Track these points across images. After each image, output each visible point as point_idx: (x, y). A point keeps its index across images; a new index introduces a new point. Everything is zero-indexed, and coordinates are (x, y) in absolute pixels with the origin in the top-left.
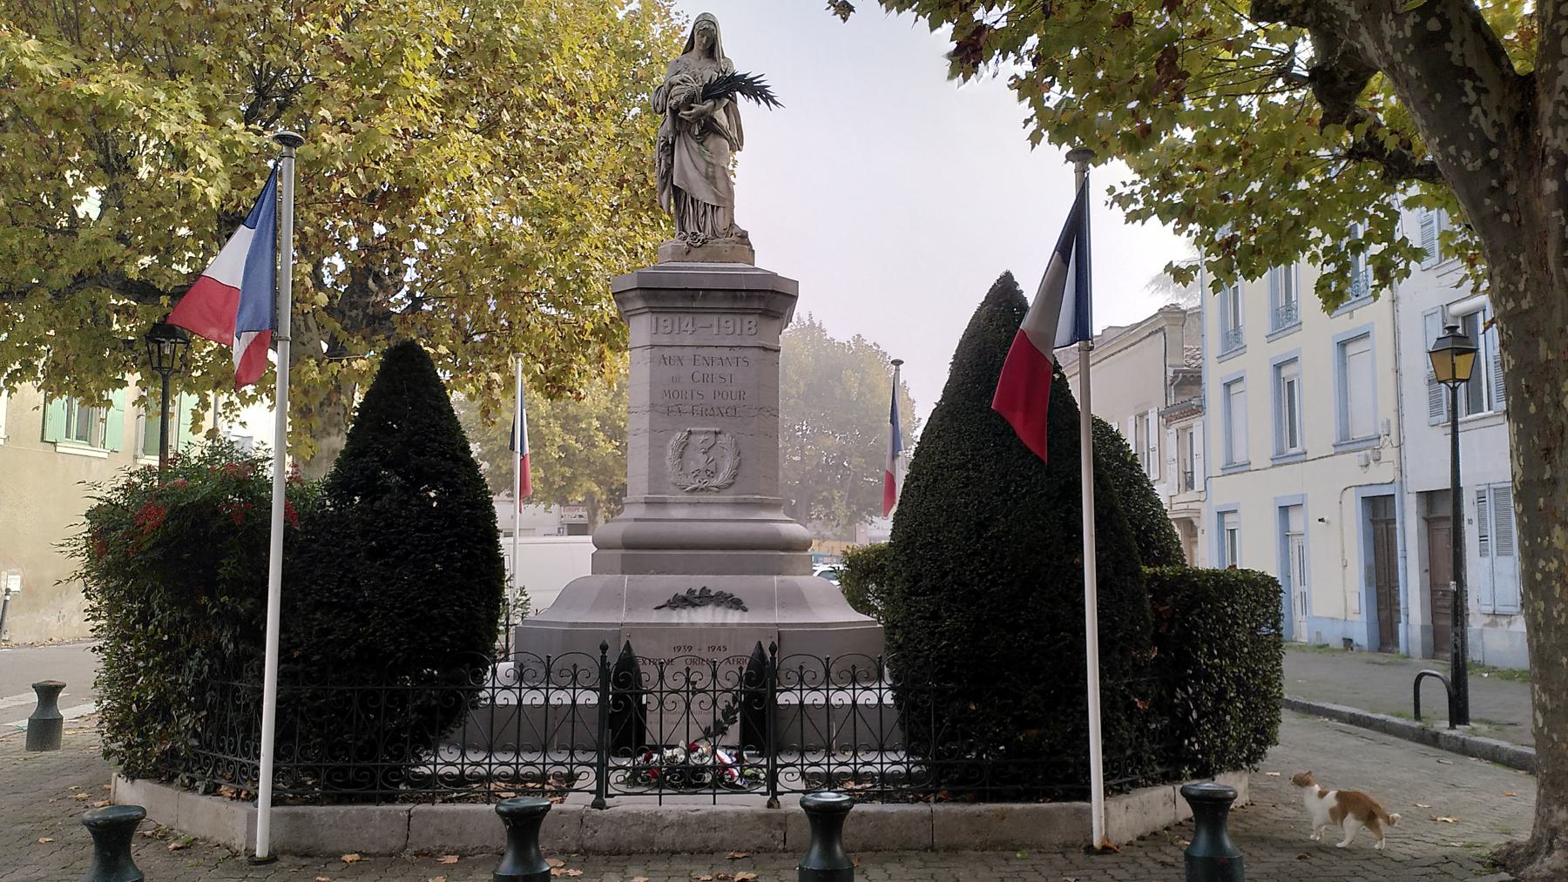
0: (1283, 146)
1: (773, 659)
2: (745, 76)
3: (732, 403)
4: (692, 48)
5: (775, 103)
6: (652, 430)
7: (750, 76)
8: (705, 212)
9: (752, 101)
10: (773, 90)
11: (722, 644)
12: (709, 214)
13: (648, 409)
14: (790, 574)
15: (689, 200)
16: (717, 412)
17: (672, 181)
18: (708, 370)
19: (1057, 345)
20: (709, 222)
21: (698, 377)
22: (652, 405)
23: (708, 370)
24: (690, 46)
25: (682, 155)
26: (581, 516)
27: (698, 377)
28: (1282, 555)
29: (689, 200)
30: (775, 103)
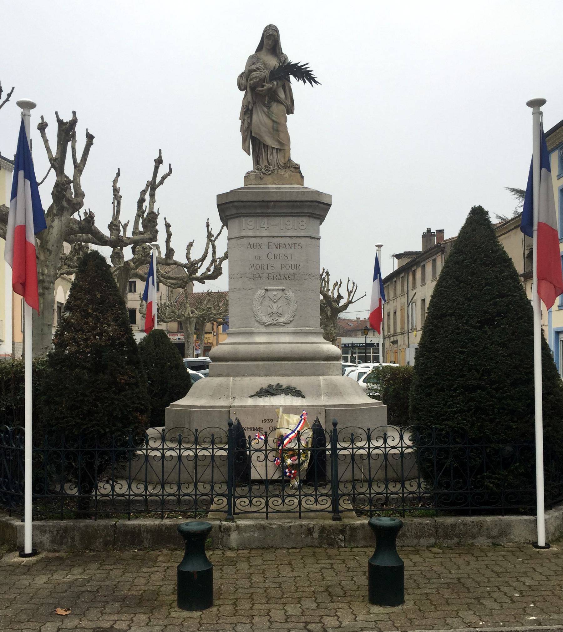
3: (291, 271)
5: (316, 82)
7: (300, 64)
9: (301, 82)
11: (271, 418)
16: (283, 277)
21: (271, 256)
23: (277, 251)
26: (179, 339)
27: (271, 256)
30: (316, 82)
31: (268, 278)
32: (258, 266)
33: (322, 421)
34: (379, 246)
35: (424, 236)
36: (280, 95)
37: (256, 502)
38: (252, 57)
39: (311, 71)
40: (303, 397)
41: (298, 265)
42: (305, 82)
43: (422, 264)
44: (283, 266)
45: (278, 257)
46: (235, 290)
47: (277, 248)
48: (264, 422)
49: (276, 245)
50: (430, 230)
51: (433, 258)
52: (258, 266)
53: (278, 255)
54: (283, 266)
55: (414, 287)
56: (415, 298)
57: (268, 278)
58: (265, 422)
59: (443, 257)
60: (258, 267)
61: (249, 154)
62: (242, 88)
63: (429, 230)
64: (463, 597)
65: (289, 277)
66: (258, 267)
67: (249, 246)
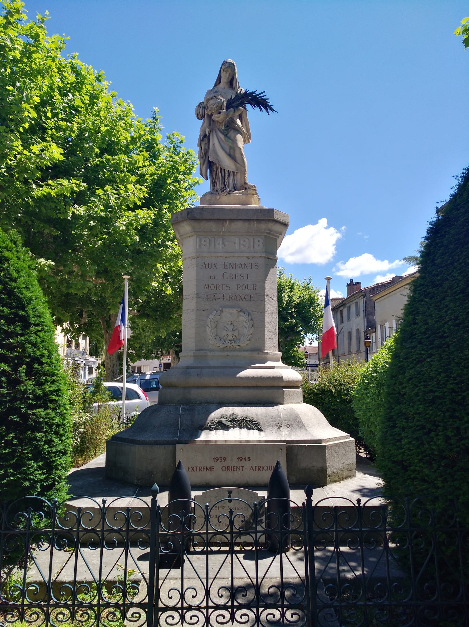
0: (372, 376)
1: (95, 622)
2: (253, 93)
3: (247, 292)
4: (220, 82)
5: (271, 109)
6: (198, 310)
7: (256, 93)
8: (229, 176)
9: (258, 109)
10: (270, 102)
11: (223, 456)
12: (231, 177)
13: (195, 296)
14: (289, 403)
15: (219, 170)
16: (238, 297)
17: (208, 159)
18: (233, 271)
19: (237, 555)
20: (231, 182)
21: (226, 276)
22: (198, 294)
23: (233, 271)
24: (218, 82)
25: (214, 141)
26: (169, 360)
27: (226, 276)
28: (357, 343)
29: (219, 170)
30: (271, 109)
31: (224, 299)
32: (212, 286)
33: (284, 470)
34: (329, 279)
35: (348, 285)
36: (238, 123)
37: (191, 618)
38: (209, 92)
39: (267, 99)
40: (260, 430)
41: (254, 286)
42: (261, 110)
43: (347, 305)
44: (239, 287)
45: (234, 277)
46: (189, 311)
47: (233, 268)
48: (215, 460)
49: (232, 265)
50: (352, 281)
51: (356, 301)
52: (212, 286)
53: (234, 275)
54: (239, 287)
55: (349, 318)
56: (342, 331)
57: (224, 299)
58: (217, 460)
59: (364, 299)
60: (213, 288)
61: (207, 179)
62: (200, 117)
63: (351, 281)
64: (125, 136)
65: (245, 298)
66: (213, 288)
67: (204, 266)
